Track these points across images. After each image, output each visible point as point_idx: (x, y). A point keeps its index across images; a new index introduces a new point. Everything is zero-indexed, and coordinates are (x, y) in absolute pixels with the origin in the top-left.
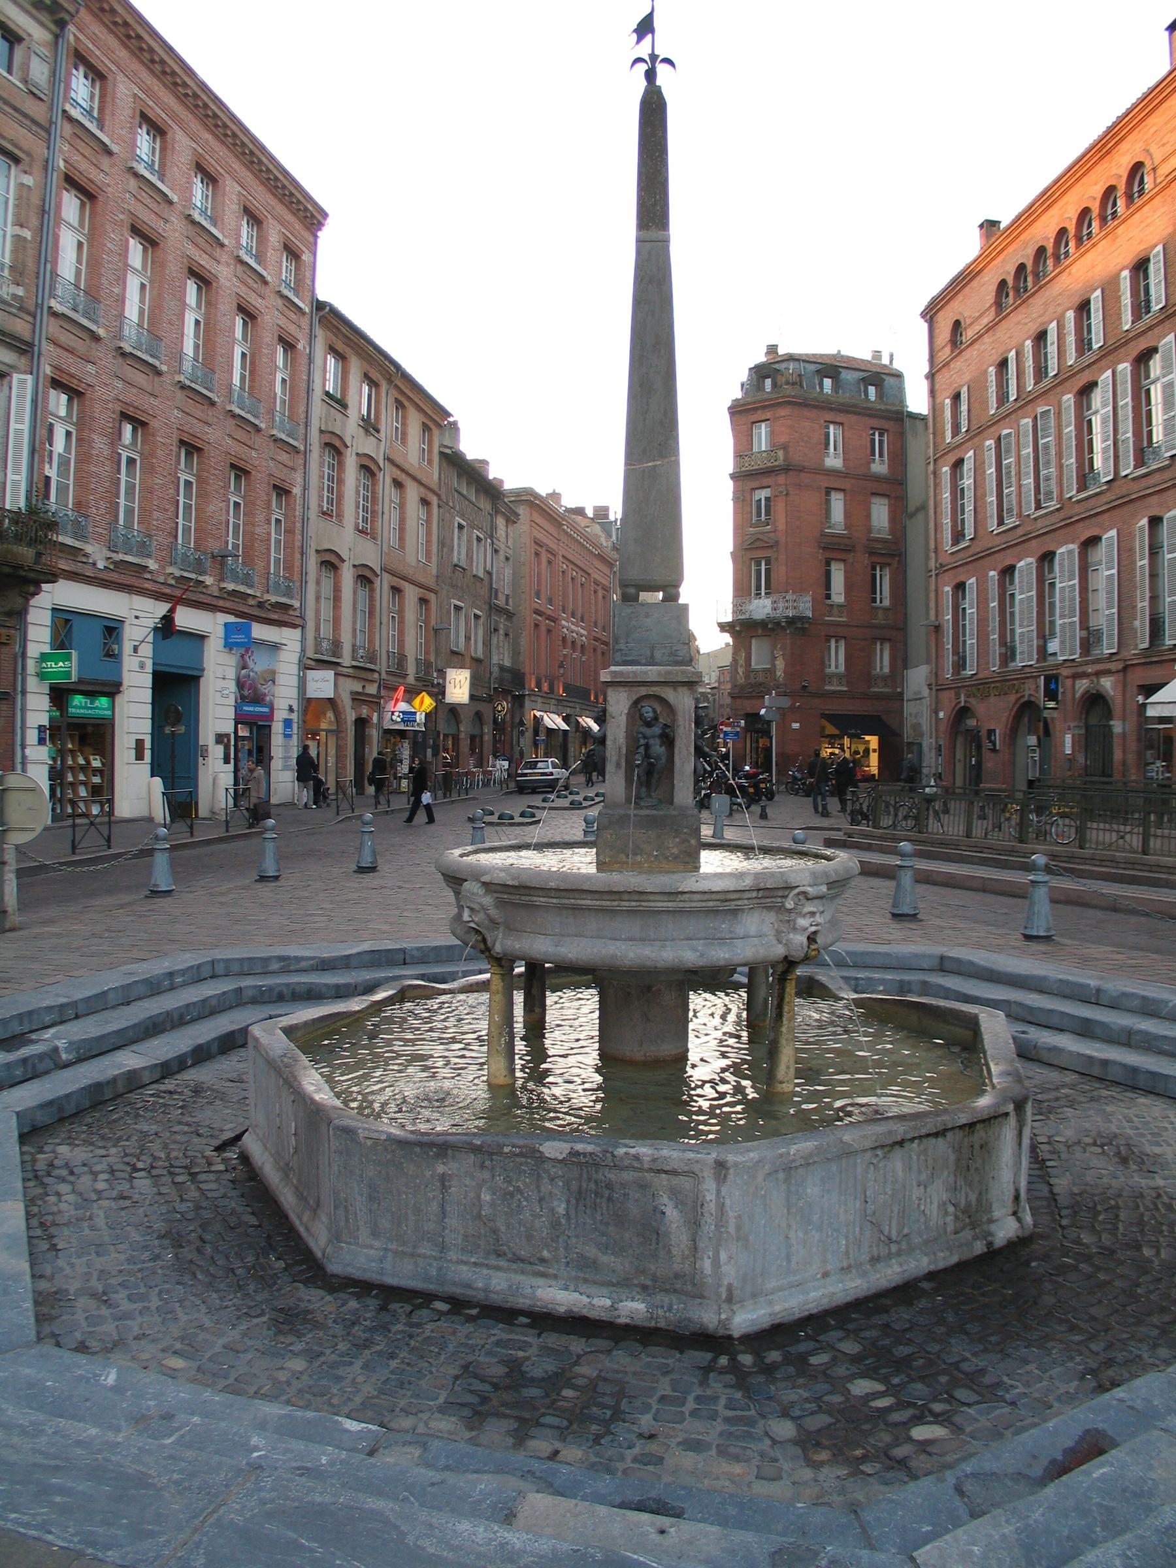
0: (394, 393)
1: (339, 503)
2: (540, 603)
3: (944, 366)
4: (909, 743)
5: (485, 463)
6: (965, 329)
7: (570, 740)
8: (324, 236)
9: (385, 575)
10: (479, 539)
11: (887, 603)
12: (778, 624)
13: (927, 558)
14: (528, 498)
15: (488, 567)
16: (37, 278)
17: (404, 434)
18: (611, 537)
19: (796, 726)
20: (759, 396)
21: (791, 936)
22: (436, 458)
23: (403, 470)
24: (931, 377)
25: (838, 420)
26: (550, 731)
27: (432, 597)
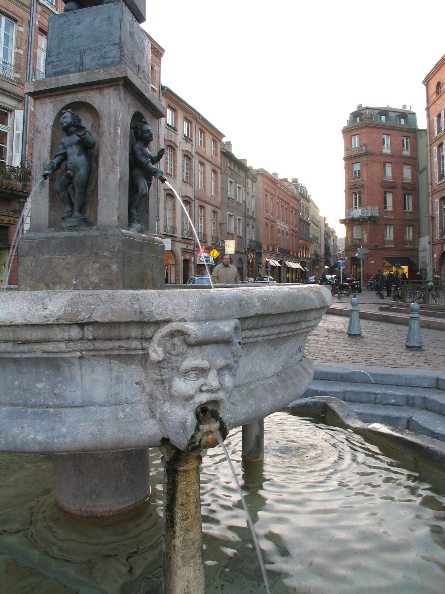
0: (199, 126)
1: (174, 170)
2: (268, 215)
3: (433, 103)
4: (420, 269)
5: (245, 160)
6: (442, 85)
7: (282, 270)
8: (164, 59)
9: (197, 201)
10: (239, 188)
11: (411, 210)
12: (364, 219)
13: (428, 188)
14: (263, 173)
15: (244, 199)
16: (26, 70)
17: (204, 143)
18: (298, 189)
19: (372, 262)
20: (354, 125)
21: (167, 407)
22: (219, 154)
23: (204, 158)
24: (428, 109)
25: (388, 133)
26: (273, 267)
27: (219, 211)
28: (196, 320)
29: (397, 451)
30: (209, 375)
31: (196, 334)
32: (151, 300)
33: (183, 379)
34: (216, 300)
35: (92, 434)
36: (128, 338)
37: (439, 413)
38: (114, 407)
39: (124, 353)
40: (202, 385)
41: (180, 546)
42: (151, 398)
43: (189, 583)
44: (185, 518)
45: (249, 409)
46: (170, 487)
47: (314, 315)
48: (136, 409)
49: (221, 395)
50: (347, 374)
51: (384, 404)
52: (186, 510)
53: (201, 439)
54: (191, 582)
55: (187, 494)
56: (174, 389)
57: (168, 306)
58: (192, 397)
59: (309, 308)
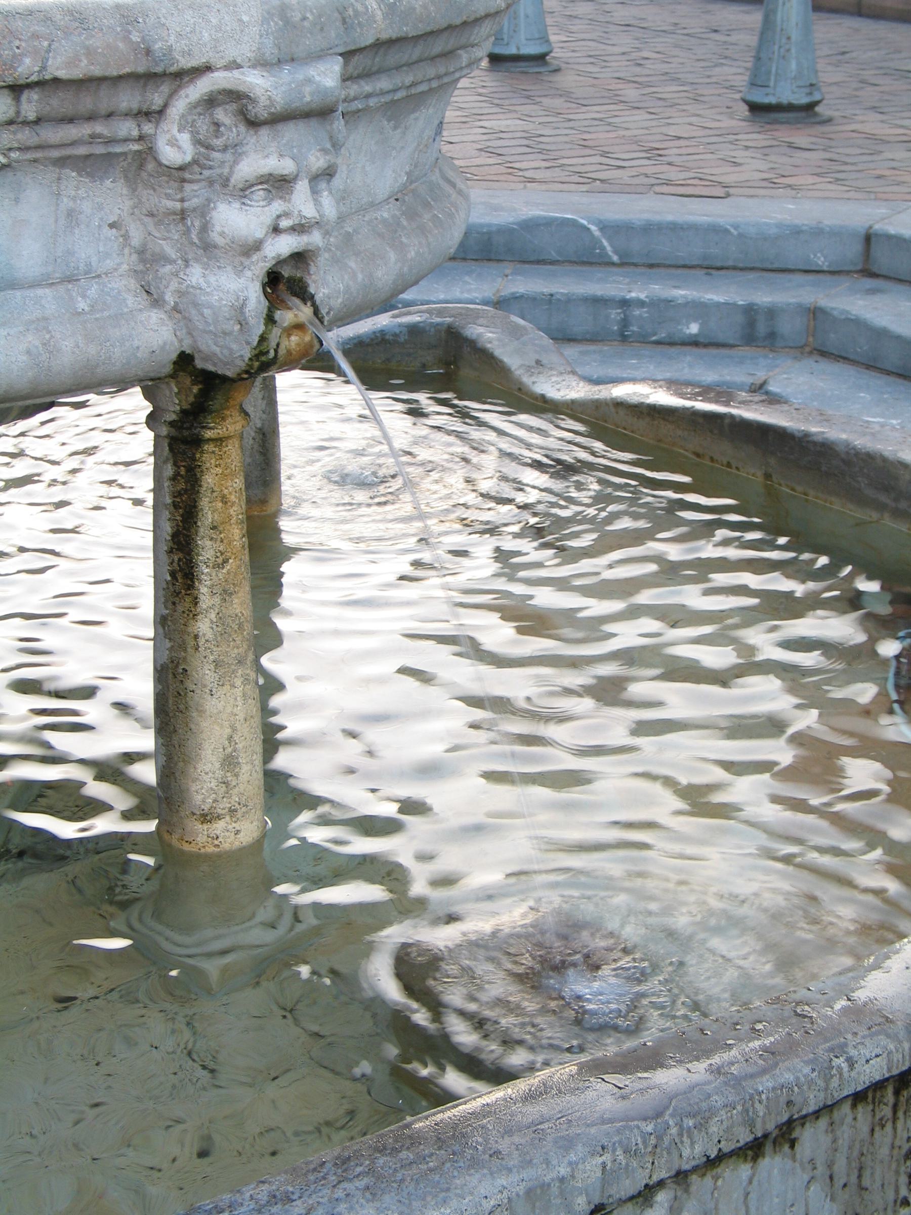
21: (196, 275)
28: (261, 63)
29: (712, 460)
30: (295, 192)
31: (270, 98)
32: (163, 20)
33: (237, 205)
34: (293, 11)
35: (28, 352)
36: (110, 115)
37: (868, 367)
38: (61, 288)
39: (100, 150)
40: (279, 217)
41: (210, 635)
42: (143, 261)
43: (234, 729)
44: (220, 560)
45: (351, 283)
46: (182, 486)
47: (488, 29)
48: (112, 289)
49: (315, 238)
50: (505, 231)
51: (658, 343)
52: (222, 541)
53: (278, 345)
54: (239, 727)
55: (224, 500)
56: (218, 228)
57: (201, 32)
58: (257, 246)
59: (483, 14)
